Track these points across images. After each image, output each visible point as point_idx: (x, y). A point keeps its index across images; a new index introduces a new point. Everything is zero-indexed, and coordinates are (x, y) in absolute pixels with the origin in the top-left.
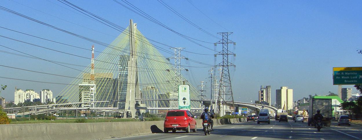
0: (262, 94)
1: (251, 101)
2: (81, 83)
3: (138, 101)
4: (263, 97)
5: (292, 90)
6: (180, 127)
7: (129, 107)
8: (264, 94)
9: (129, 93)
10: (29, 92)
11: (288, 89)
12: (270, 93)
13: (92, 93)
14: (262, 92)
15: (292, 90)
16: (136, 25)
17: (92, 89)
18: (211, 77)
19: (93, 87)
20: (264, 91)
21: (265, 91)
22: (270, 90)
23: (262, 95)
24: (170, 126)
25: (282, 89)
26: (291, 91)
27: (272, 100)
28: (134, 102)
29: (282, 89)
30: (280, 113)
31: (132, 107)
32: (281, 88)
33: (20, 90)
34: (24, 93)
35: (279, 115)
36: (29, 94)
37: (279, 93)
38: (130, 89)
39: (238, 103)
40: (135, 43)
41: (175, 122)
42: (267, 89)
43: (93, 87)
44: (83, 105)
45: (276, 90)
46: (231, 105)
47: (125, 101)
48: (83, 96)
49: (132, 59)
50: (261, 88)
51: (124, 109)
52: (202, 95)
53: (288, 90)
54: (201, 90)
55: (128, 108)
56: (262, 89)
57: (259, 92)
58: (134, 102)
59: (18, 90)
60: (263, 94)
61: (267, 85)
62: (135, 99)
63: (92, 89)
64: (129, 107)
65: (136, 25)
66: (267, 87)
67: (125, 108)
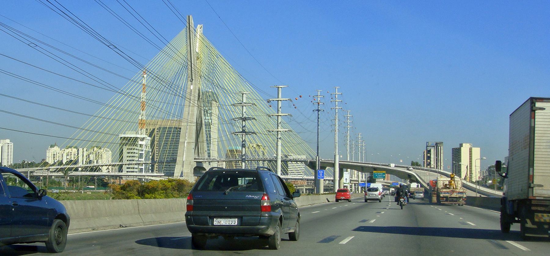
0: (429, 155)
1: (401, 161)
2: (124, 134)
3: (201, 162)
4: (430, 161)
5: (479, 148)
6: (345, 198)
7: (182, 172)
8: (432, 156)
9: (183, 146)
10: (70, 149)
11: (473, 147)
12: (442, 155)
13: (142, 151)
14: (429, 152)
15: (479, 148)
16: (201, 28)
17: (140, 142)
18: (318, 110)
19: (143, 139)
20: (432, 151)
21: (434, 151)
22: (442, 149)
23: (429, 158)
24: (340, 198)
25: (462, 148)
26: (476, 152)
27: (445, 165)
28: (190, 163)
29: (462, 146)
30: (414, 189)
31: (187, 173)
32: (461, 145)
33: (55, 147)
34: (61, 152)
35: (412, 190)
36: (70, 153)
37: (456, 153)
38: (186, 140)
39: (366, 164)
40: (198, 58)
41: (343, 196)
42: (436, 147)
43: (143, 139)
44: (124, 167)
45: (453, 149)
46: (362, 169)
47: (176, 162)
48: (125, 154)
49: (192, 86)
50: (427, 146)
51: (173, 176)
52: (244, 131)
53: (473, 148)
54: (243, 115)
55: (180, 175)
56: (428, 148)
57: (424, 152)
58: (190, 163)
59: (52, 146)
60: (430, 155)
61: (438, 141)
62: (195, 159)
63: (140, 142)
64: (182, 172)
65: (201, 28)
66: (437, 144)
67: (174, 174)
